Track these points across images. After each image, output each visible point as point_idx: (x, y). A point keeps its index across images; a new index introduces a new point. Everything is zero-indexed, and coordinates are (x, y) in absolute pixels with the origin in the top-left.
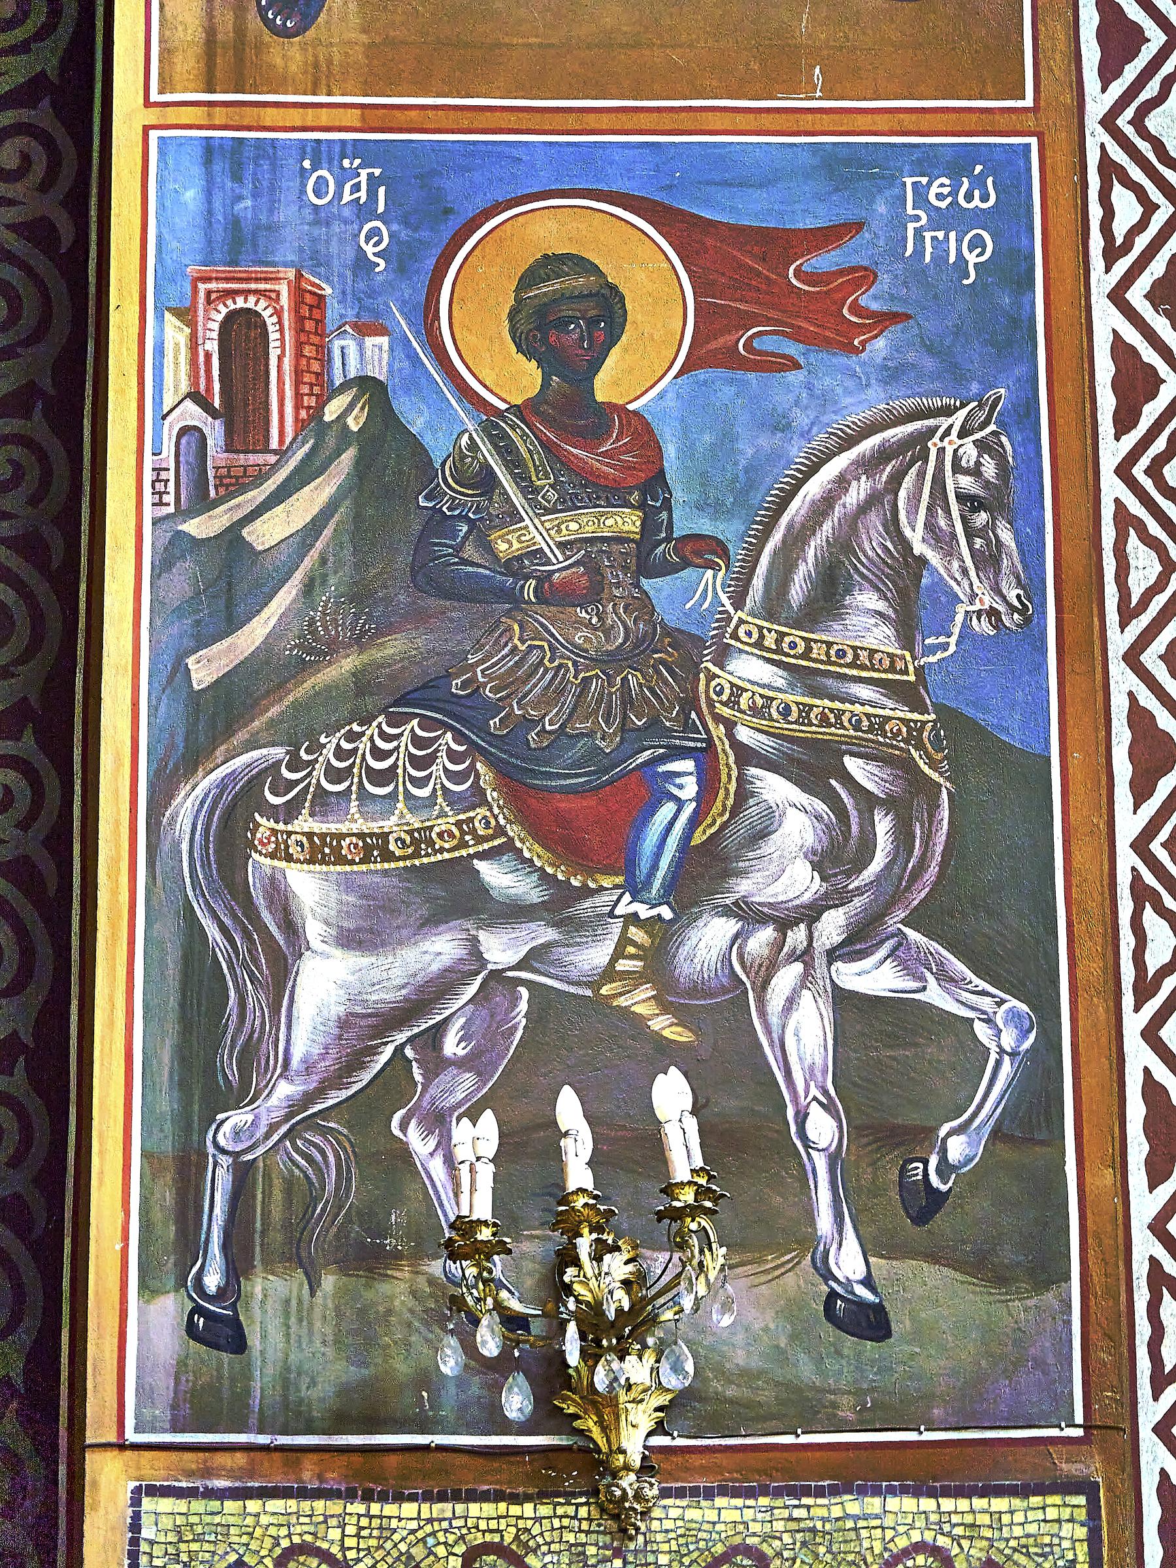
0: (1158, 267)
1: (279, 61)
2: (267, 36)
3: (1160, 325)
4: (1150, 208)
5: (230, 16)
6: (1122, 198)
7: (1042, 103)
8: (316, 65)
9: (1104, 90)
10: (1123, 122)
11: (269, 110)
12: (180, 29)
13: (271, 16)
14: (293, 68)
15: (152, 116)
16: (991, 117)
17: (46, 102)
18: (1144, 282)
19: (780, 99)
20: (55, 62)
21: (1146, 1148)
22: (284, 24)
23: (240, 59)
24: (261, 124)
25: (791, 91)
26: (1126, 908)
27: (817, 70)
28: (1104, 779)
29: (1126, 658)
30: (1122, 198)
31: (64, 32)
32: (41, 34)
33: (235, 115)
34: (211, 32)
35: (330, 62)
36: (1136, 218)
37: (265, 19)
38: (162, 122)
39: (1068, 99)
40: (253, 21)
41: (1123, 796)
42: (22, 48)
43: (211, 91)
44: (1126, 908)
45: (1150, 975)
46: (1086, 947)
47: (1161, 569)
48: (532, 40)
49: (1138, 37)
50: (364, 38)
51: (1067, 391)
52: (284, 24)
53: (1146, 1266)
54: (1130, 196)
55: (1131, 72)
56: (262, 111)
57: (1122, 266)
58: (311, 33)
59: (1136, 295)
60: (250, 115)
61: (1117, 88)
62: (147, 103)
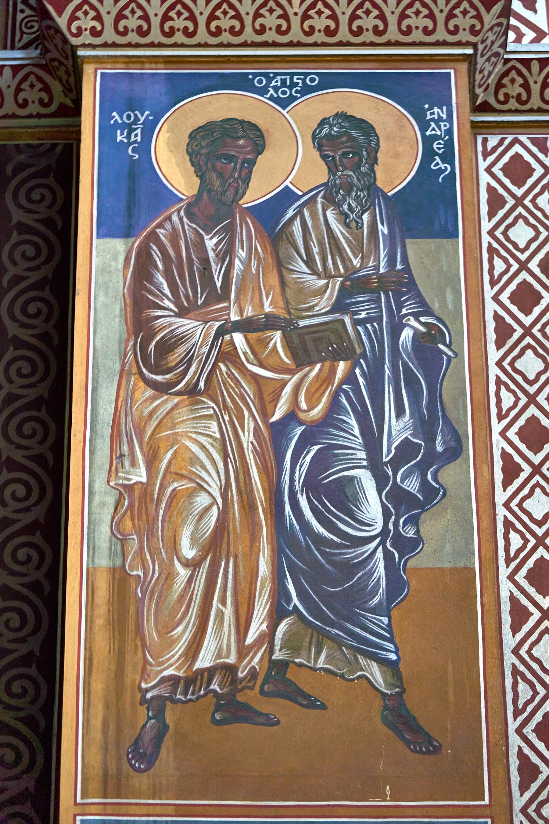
0: (538, 717)
1: (137, 784)
2: (132, 772)
3: (541, 746)
4: (526, 541)
5: (114, 763)
6: (522, 686)
7: (493, 803)
8: (154, 786)
9: (521, 795)
10: (505, 364)
11: (133, 807)
12: (91, 769)
13: (133, 762)
14: (144, 787)
15: (78, 810)
16: (469, 809)
17: (28, 803)
18: (532, 724)
19: (371, 801)
20: (33, 783)
21: (501, 463)
22: (140, 766)
23: (119, 780)
24: (129, 813)
25: (374, 799)
26: (509, 681)
27: (388, 787)
28: (485, 367)
29: (516, 731)
30: (522, 686)
31: (36, 773)
32: (41, 380)
33: (116, 809)
34: (105, 774)
35: (160, 784)
36: (511, 404)
37: (130, 764)
38: (82, 812)
39: (505, 800)
40: (125, 766)
41: (491, 347)
42: (17, 777)
43: (105, 797)
44: (509, 681)
45: (495, 256)
46: (484, 504)
47: (532, 693)
48: (255, 774)
49: (536, 771)
50: (177, 773)
51: (488, 583)
52: (140, 766)
53: (502, 520)
54: (518, 536)
55: (534, 787)
56: (129, 807)
57: (505, 422)
58: (152, 770)
59: (504, 297)
60: (123, 809)
61: (527, 795)
62: (75, 803)
